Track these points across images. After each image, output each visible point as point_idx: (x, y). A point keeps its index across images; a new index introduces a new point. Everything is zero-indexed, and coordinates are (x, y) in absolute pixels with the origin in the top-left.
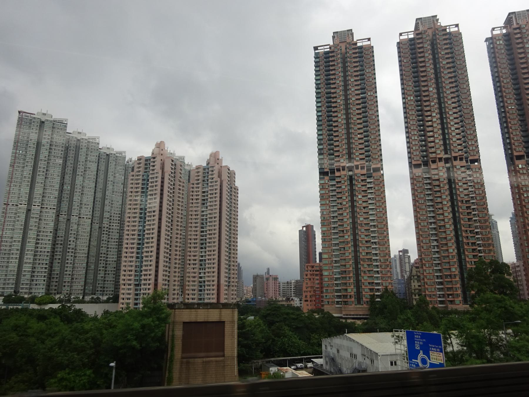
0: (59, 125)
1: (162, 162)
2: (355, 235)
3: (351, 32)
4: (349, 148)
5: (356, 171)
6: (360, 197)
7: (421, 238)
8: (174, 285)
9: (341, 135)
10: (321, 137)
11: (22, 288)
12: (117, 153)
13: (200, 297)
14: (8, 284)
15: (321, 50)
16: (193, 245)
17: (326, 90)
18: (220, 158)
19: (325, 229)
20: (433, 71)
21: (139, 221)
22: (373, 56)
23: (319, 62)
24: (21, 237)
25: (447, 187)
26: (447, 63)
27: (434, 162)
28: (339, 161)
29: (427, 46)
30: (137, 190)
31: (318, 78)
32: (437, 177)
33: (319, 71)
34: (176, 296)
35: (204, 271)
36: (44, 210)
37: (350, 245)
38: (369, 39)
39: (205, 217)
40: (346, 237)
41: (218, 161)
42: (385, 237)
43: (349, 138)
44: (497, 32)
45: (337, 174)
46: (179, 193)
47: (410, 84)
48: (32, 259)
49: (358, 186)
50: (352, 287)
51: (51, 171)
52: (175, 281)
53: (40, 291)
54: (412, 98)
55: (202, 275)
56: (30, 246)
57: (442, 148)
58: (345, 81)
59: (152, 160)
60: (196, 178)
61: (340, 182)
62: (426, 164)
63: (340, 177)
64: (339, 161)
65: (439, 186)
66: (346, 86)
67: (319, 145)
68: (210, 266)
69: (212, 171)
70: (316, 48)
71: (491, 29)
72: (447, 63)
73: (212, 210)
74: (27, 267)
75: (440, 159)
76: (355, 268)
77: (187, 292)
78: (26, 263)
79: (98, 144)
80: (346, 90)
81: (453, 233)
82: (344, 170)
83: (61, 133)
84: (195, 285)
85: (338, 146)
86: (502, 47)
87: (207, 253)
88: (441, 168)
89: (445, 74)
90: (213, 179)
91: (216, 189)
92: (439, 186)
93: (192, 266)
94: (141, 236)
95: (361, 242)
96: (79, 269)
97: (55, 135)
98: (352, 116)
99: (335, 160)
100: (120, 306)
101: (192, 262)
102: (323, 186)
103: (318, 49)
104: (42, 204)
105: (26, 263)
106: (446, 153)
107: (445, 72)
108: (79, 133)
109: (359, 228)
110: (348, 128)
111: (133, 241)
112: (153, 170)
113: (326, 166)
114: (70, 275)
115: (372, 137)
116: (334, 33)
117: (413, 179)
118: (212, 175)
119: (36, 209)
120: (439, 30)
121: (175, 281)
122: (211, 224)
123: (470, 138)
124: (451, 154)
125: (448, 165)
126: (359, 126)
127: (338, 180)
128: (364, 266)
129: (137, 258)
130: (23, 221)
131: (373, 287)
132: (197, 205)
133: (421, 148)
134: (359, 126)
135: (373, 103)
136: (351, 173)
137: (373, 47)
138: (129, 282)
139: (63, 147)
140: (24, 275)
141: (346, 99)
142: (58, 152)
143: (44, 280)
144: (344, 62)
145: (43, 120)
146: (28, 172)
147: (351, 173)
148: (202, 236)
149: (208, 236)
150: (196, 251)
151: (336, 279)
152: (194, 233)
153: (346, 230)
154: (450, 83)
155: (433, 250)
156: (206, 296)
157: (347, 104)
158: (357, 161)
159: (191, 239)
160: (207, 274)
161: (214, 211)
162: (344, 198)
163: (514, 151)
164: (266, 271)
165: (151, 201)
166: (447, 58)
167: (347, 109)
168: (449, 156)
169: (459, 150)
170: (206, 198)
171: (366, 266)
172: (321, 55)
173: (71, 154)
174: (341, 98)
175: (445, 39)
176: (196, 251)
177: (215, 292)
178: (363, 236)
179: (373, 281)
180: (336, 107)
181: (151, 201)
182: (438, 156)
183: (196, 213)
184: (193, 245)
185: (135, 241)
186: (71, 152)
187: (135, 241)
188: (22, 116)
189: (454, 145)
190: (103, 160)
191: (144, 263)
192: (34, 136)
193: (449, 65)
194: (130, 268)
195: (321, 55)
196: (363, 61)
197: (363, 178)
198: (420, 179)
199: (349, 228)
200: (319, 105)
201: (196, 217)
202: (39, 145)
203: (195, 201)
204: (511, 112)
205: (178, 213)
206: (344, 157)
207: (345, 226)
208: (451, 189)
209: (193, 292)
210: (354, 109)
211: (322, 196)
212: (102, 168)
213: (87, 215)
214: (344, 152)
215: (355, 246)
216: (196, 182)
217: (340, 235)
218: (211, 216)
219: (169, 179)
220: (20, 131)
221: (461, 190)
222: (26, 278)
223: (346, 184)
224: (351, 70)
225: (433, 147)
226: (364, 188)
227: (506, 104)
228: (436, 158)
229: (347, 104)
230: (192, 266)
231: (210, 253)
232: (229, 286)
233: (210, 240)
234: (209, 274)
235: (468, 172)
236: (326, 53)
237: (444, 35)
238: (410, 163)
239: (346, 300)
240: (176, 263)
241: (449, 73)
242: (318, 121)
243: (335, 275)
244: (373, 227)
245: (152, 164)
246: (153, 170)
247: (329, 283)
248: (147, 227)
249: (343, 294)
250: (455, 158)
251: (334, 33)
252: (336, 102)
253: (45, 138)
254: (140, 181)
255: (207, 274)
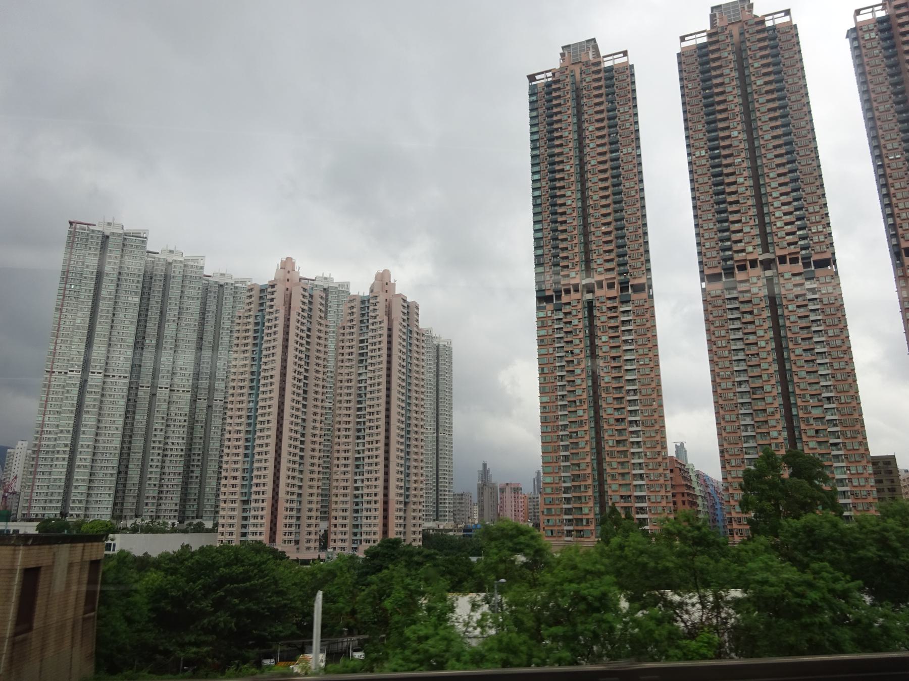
0: (131, 241)
1: (288, 293)
2: (597, 408)
3: (593, 43)
4: (587, 252)
5: (598, 292)
6: (604, 339)
7: (722, 412)
8: (311, 502)
9: (572, 229)
10: (540, 235)
11: (73, 509)
12: (236, 282)
13: (356, 523)
14: (51, 501)
15: (541, 80)
16: (343, 433)
17: (549, 151)
18: (392, 281)
19: (546, 399)
20: (738, 100)
21: (250, 394)
22: (633, 83)
23: (537, 101)
24: (71, 425)
25: (767, 313)
26: (766, 83)
27: (742, 268)
28: (568, 276)
29: (728, 55)
30: (247, 341)
31: (535, 129)
32: (747, 297)
33: (537, 117)
34: (313, 521)
35: (361, 477)
36: (108, 380)
37: (586, 428)
38: (625, 53)
39: (363, 384)
40: (580, 413)
41: (386, 288)
42: (655, 411)
43: (586, 234)
44: (865, 17)
45: (565, 299)
46: (319, 344)
47: (700, 127)
48: (88, 460)
49: (601, 318)
50: (591, 504)
51: (120, 315)
52: (311, 495)
53: (102, 512)
54: (703, 153)
55: (359, 484)
56: (86, 439)
57: (758, 241)
58: (580, 131)
59: (270, 290)
60: (349, 318)
61: (570, 313)
62: (729, 272)
63: (569, 304)
64: (568, 276)
65: (751, 312)
66: (581, 139)
67: (537, 248)
68: (370, 468)
69: (375, 304)
70: (532, 78)
71: (853, 13)
72: (766, 83)
73: (374, 371)
74: (80, 474)
75: (753, 263)
76: (598, 470)
77: (334, 514)
78: (79, 467)
79: (202, 268)
80: (581, 147)
81: (780, 400)
82: (576, 290)
83: (137, 252)
84: (346, 502)
85: (566, 249)
86: (875, 44)
87: (367, 446)
88: (755, 280)
89: (762, 104)
90: (375, 317)
91: (380, 336)
92: (751, 312)
93: (342, 469)
94: (252, 418)
95: (607, 421)
96: (172, 476)
97: (126, 257)
98: (591, 193)
99: (562, 273)
100: (215, 541)
101: (343, 462)
102: (542, 322)
103: (536, 80)
104: (106, 370)
105: (79, 467)
106: (766, 250)
107: (761, 101)
108: (171, 252)
109: (603, 395)
110: (585, 216)
111: (239, 428)
112: (271, 307)
113: (548, 287)
114: (155, 485)
115: (631, 229)
116: (563, 48)
117: (707, 302)
118: (375, 310)
119: (95, 379)
120: (750, 23)
121: (311, 495)
122: (372, 395)
123: (813, 219)
124: (774, 253)
125: (769, 273)
126: (604, 211)
127: (567, 309)
128: (612, 466)
129: (246, 455)
130: (76, 399)
131: (629, 505)
132: (350, 364)
133: (720, 244)
134: (604, 211)
135: (631, 166)
136: (589, 296)
137: (632, 66)
138: (233, 497)
139: (139, 275)
140: (77, 487)
141: (582, 163)
142: (133, 285)
143: (109, 495)
144: (578, 98)
145: (107, 233)
146: (82, 318)
147: (589, 296)
148: (359, 417)
149: (368, 417)
150: (348, 444)
151: (567, 490)
152: (345, 412)
153: (580, 401)
154: (771, 119)
155: (744, 434)
156: (365, 521)
157: (582, 173)
158: (600, 274)
159: (340, 423)
160: (366, 483)
161: (377, 373)
162: (577, 342)
163: (902, 240)
164: (535, 476)
165: (267, 360)
166: (765, 74)
167: (583, 181)
168: (772, 256)
169: (789, 244)
170: (365, 351)
171: (615, 465)
172: (540, 89)
173: (157, 287)
174: (572, 162)
175: (760, 40)
176: (348, 444)
177: (379, 513)
178: (610, 411)
179: (629, 493)
180: (563, 179)
181: (267, 360)
182: (750, 257)
183: (349, 377)
184: (343, 433)
185: (242, 428)
186: (158, 283)
187: (242, 428)
188: (75, 228)
189: (779, 235)
190: (212, 294)
191: (256, 465)
192: (92, 261)
193: (769, 87)
194: (235, 474)
195: (540, 89)
196: (614, 93)
197: (610, 304)
198: (720, 302)
199: (585, 396)
200: (537, 177)
201: (349, 384)
202: (99, 276)
203: (347, 357)
204: (894, 165)
205: (317, 378)
206: (577, 268)
207: (578, 392)
208: (775, 317)
209: (344, 514)
210: (595, 179)
211: (542, 341)
212: (212, 307)
213: (184, 386)
214: (577, 259)
215: (598, 429)
216: (349, 324)
217: (570, 409)
218: (373, 382)
219: (298, 321)
220: (71, 253)
221: (793, 318)
222: (78, 493)
223: (580, 316)
224: (589, 111)
225: (740, 241)
226: (613, 323)
227: (884, 152)
228: (745, 260)
229: (582, 173)
230: (342, 469)
231: (371, 446)
232: (406, 504)
233: (371, 424)
234: (369, 483)
235: (809, 285)
236: (548, 85)
237: (758, 32)
238: (702, 272)
239: (580, 528)
240: (313, 465)
241: (768, 101)
242: (535, 206)
243: (564, 482)
244: (632, 393)
245: (371, 308)
246: (271, 307)
247: (555, 496)
248: (260, 404)
249: (576, 517)
250: (782, 260)
251: (563, 48)
252: (563, 170)
253: (109, 263)
254: (251, 327)
255: (366, 483)
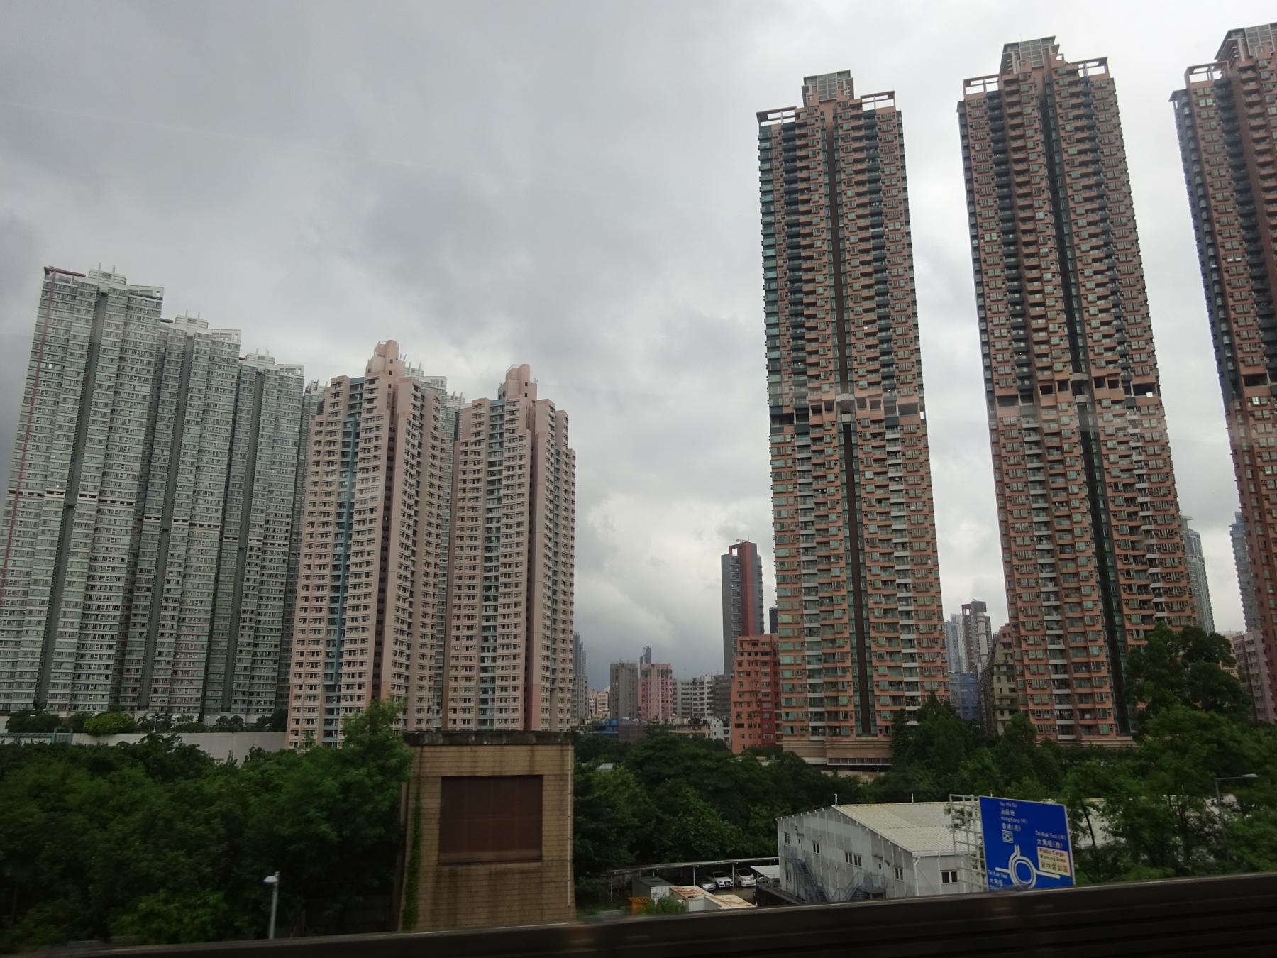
0: (142, 302)
1: (391, 391)
2: (856, 566)
3: (846, 76)
4: (843, 358)
5: (860, 413)
6: (868, 475)
7: (1017, 575)
8: (421, 688)
9: (824, 326)
10: (775, 331)
11: (54, 696)
12: (282, 369)
13: (483, 717)
14: (20, 685)
15: (774, 122)
16: (465, 592)
17: (787, 218)
18: (532, 381)
19: (783, 552)
20: (1044, 171)
21: (337, 534)
22: (901, 135)
23: (770, 149)
24: (50, 573)
25: (1079, 451)
26: (1080, 152)
27: (1047, 390)
28: (819, 389)
29: (1032, 110)
30: (332, 458)
31: (768, 187)
32: (1054, 427)
33: (770, 170)
34: (424, 715)
35: (491, 654)
36: (105, 507)
37: (844, 592)
38: (891, 95)
39: (494, 524)
40: (836, 572)
41: (526, 390)
42: (930, 571)
43: (842, 334)
44: (1199, 77)
45: (814, 419)
46: (433, 466)
47: (990, 202)
48: (77, 625)
49: (865, 449)
50: (850, 692)
51: (124, 412)
52: (422, 678)
53: (96, 702)
54: (994, 237)
55: (488, 664)
56: (73, 593)
57: (1068, 357)
58: (834, 195)
59: (367, 386)
60: (474, 430)
61: (821, 439)
62: (1028, 395)
63: (820, 426)
64: (819, 389)
65: (1059, 448)
66: (834, 206)
67: (771, 349)
68: (506, 641)
69: (513, 413)
70: (762, 116)
71: (1184, 71)
72: (1080, 152)
73: (512, 506)
74: (64, 645)
75: (1063, 384)
76: (858, 648)
77: (451, 705)
78: (63, 634)
79: (237, 347)
80: (835, 217)
81: (1094, 562)
82: (829, 409)
83: (148, 320)
84: (470, 689)
85: (816, 352)
86: (1212, 113)
87: (501, 610)
88: (1065, 406)
89: (1075, 179)
90: (513, 431)
91: (521, 457)
92: (1059, 448)
93: (464, 642)
94: (341, 569)
95: (872, 583)
96: (191, 649)
97: (132, 326)
98: (849, 280)
99: (810, 385)
100: (290, 739)
101: (464, 632)
102: (779, 449)
103: (767, 119)
104: (101, 493)
105: (63, 634)
106: (1077, 369)
107: (1074, 175)
108: (191, 321)
109: (867, 549)
110: (840, 310)
111: (321, 582)
112: (370, 410)
113: (787, 401)
114: (168, 662)
115: (899, 331)
116: (806, 79)
117: (998, 432)
118: (512, 421)
119: (86, 504)
120: (1061, 71)
121: (422, 678)
122: (509, 540)
123: (1133, 332)
124: (1088, 372)
125: (1081, 399)
126: (867, 305)
127: (816, 433)
128: (878, 642)
129: (332, 622)
130: (57, 534)
131: (900, 693)
132: (476, 495)
133: (1016, 357)
134: (867, 305)
135: (899, 247)
136: (846, 418)
137: (899, 113)
138: (312, 681)
139: (151, 354)
140: (59, 665)
141: (836, 240)
142: (141, 366)
143: (107, 676)
144: (831, 150)
145: (104, 289)
146: (67, 414)
147: (846, 418)
148: (488, 569)
149: (502, 570)
150: (473, 607)
151: (812, 674)
152: (468, 562)
153: (836, 556)
154: (1086, 200)
155: (1046, 604)
156: (497, 715)
157: (837, 252)
158: (863, 388)
159: (460, 578)
160: (499, 662)
161: (517, 510)
162: (831, 477)
163: (1241, 365)
164: (642, 653)
165: (364, 486)
166: (1078, 141)
167: (837, 263)
168: (1085, 377)
169: (1108, 363)
170: (497, 477)
171: (883, 641)
172: (775, 134)
173: (172, 372)
174: (824, 236)
175: (1073, 95)
176: (473, 607)
177: (519, 704)
178: (876, 570)
179: (899, 679)
180: (811, 258)
181: (364, 486)
182: (1058, 377)
183: (474, 514)
184: (465, 592)
185: (327, 582)
186: (172, 366)
187: (327, 582)
188: (54, 279)
189: (1096, 350)
190: (248, 386)
191: (348, 635)
192: (82, 329)
193: (1083, 158)
194: (315, 648)
195: (775, 134)
196: (876, 148)
197: (875, 429)
198: (1015, 433)
199: (842, 550)
200: (770, 252)
201: (474, 524)
202: (93, 349)
203: (471, 485)
204: (1233, 270)
205: (430, 514)
206: (832, 380)
207: (833, 544)
208: (1088, 455)
209: (467, 705)
210: (855, 262)
211: (778, 474)
212: (247, 405)
213: (210, 518)
214: (831, 367)
215: (858, 593)
216: (474, 439)
217: (821, 567)
218: (509, 521)
219: (409, 433)
220: (47, 317)
221: (1112, 458)
222: (62, 671)
223: (835, 443)
224: (847, 170)
225: (1046, 355)
226: (878, 454)
227: (1222, 252)
228: (1052, 380)
229: (837, 252)
230: (464, 642)
231: (506, 611)
232: (552, 690)
233: (507, 580)
234: (505, 662)
235: (1130, 416)
236: (787, 128)
237: (1071, 84)
238: (990, 393)
239: (834, 724)
240: (424, 636)
241: (1083, 176)
242: (768, 291)
243: (809, 663)
244: (899, 548)
245: (366, 396)
246: (370, 410)
247: (795, 682)
248: (354, 548)
249: (829, 709)
250: (1099, 382)
251: (806, 79)
252: (811, 246)
253: (108, 334)
254: (338, 438)
255: (499, 662)
